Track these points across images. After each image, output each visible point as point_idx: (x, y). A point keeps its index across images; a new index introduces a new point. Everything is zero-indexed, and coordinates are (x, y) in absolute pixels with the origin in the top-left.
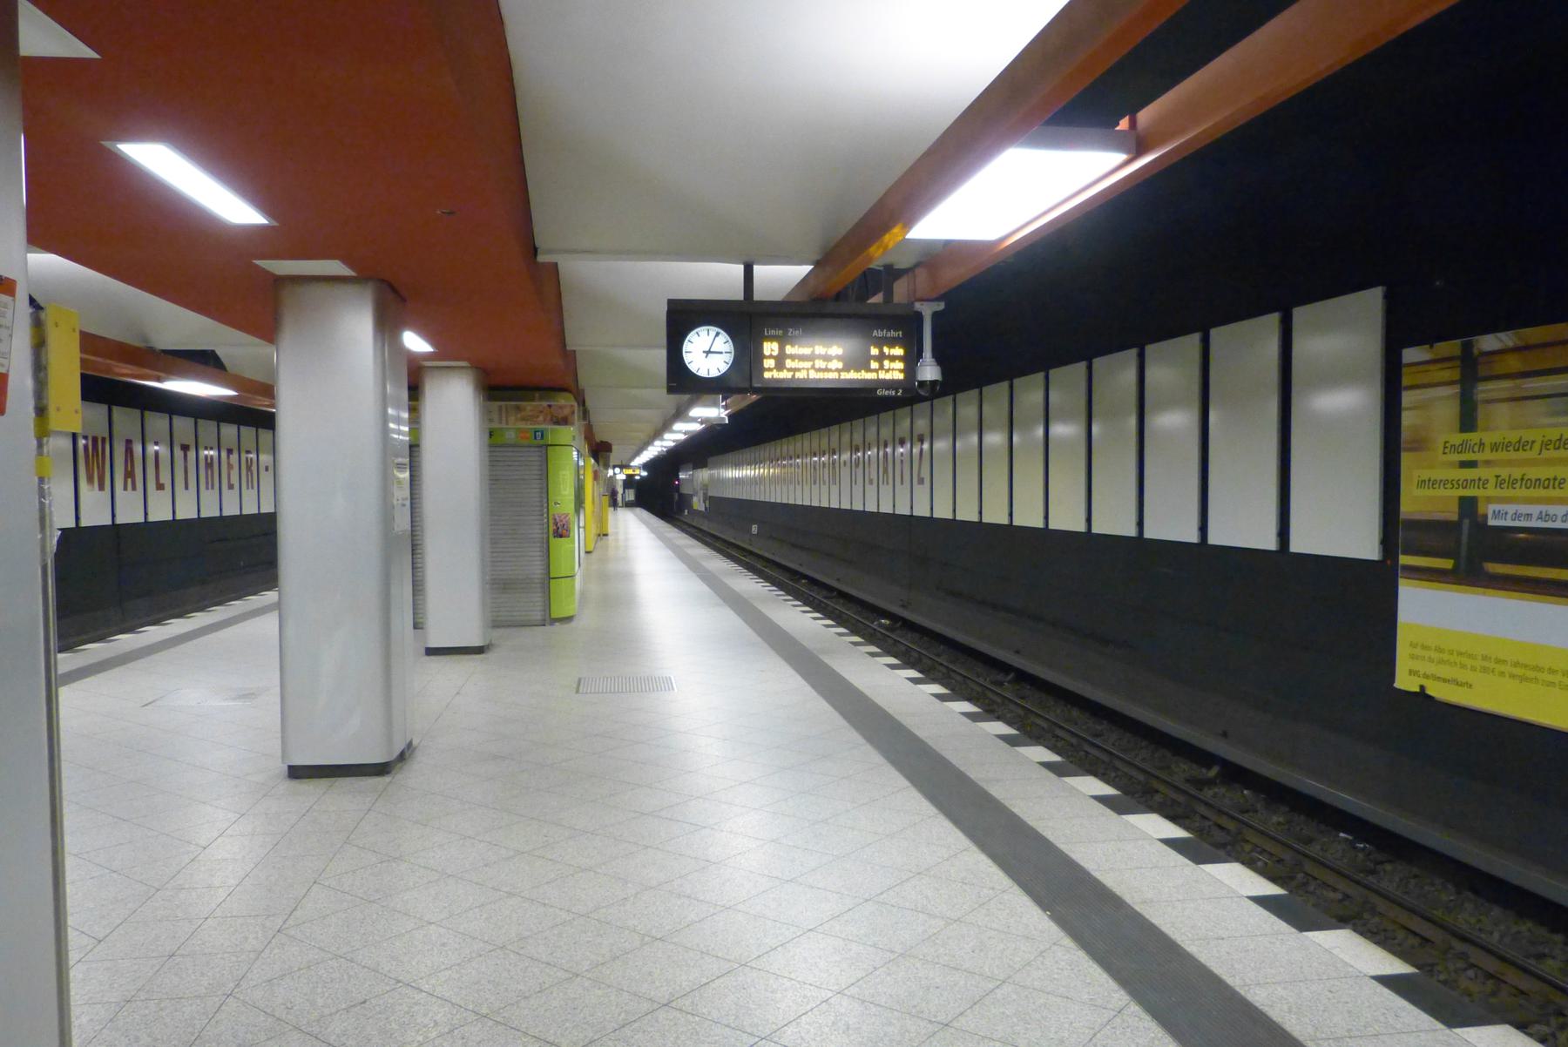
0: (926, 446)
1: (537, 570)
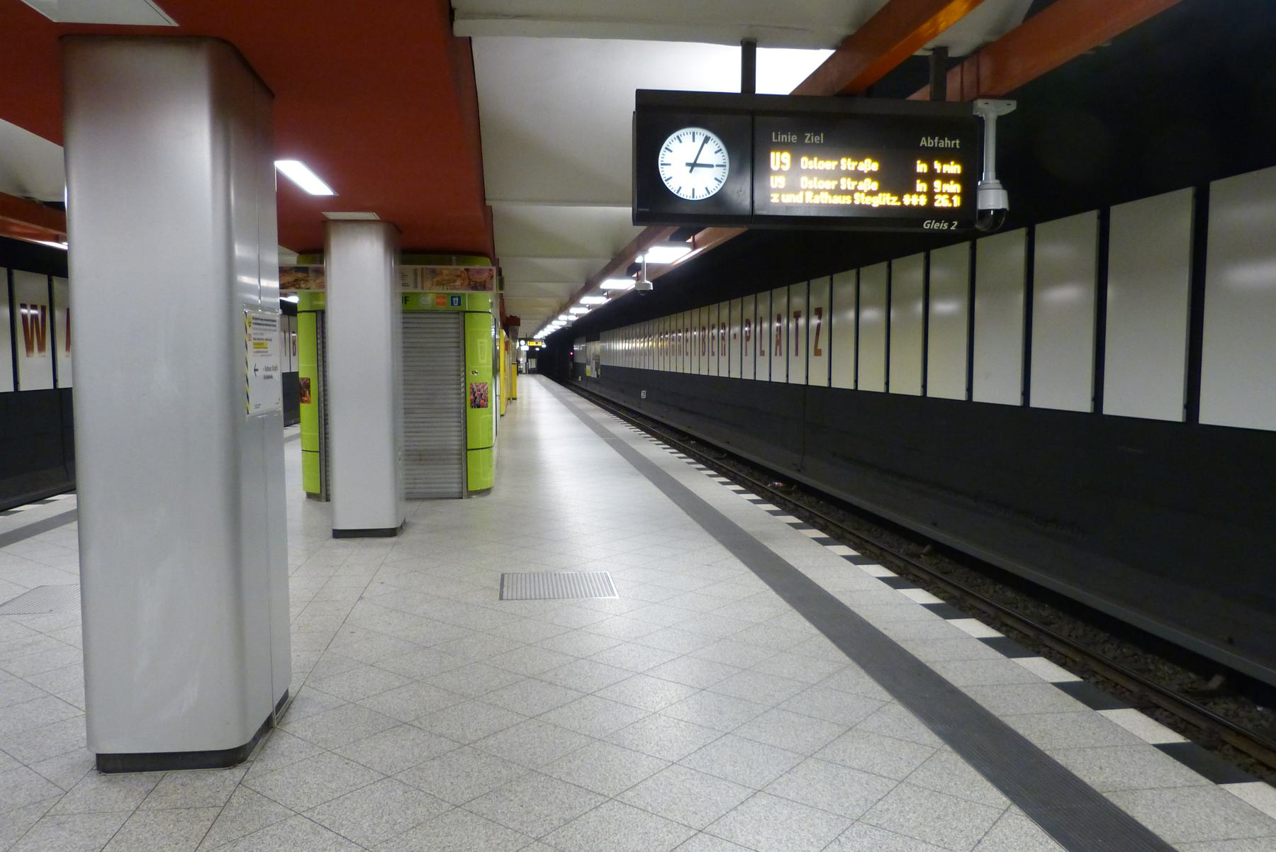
0: (802, 321)
1: (454, 442)
